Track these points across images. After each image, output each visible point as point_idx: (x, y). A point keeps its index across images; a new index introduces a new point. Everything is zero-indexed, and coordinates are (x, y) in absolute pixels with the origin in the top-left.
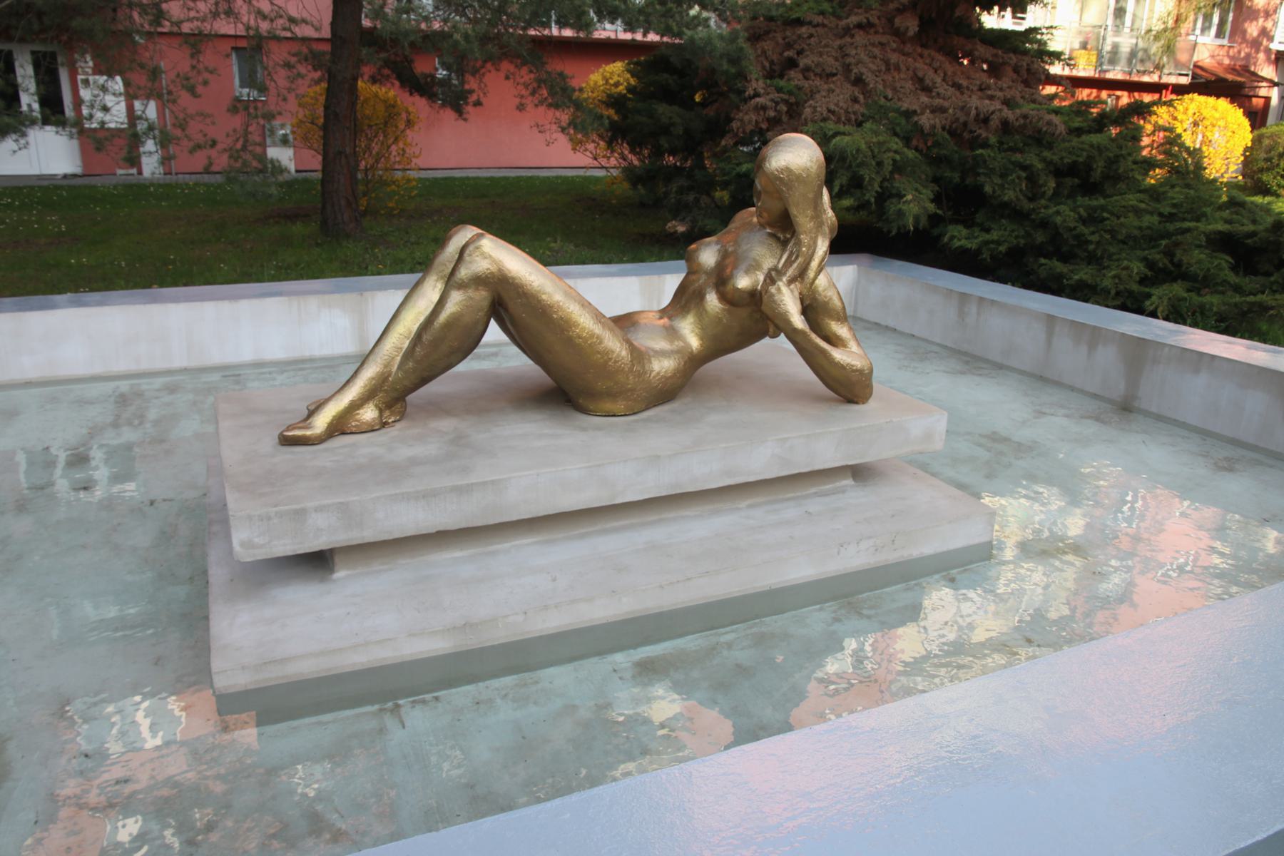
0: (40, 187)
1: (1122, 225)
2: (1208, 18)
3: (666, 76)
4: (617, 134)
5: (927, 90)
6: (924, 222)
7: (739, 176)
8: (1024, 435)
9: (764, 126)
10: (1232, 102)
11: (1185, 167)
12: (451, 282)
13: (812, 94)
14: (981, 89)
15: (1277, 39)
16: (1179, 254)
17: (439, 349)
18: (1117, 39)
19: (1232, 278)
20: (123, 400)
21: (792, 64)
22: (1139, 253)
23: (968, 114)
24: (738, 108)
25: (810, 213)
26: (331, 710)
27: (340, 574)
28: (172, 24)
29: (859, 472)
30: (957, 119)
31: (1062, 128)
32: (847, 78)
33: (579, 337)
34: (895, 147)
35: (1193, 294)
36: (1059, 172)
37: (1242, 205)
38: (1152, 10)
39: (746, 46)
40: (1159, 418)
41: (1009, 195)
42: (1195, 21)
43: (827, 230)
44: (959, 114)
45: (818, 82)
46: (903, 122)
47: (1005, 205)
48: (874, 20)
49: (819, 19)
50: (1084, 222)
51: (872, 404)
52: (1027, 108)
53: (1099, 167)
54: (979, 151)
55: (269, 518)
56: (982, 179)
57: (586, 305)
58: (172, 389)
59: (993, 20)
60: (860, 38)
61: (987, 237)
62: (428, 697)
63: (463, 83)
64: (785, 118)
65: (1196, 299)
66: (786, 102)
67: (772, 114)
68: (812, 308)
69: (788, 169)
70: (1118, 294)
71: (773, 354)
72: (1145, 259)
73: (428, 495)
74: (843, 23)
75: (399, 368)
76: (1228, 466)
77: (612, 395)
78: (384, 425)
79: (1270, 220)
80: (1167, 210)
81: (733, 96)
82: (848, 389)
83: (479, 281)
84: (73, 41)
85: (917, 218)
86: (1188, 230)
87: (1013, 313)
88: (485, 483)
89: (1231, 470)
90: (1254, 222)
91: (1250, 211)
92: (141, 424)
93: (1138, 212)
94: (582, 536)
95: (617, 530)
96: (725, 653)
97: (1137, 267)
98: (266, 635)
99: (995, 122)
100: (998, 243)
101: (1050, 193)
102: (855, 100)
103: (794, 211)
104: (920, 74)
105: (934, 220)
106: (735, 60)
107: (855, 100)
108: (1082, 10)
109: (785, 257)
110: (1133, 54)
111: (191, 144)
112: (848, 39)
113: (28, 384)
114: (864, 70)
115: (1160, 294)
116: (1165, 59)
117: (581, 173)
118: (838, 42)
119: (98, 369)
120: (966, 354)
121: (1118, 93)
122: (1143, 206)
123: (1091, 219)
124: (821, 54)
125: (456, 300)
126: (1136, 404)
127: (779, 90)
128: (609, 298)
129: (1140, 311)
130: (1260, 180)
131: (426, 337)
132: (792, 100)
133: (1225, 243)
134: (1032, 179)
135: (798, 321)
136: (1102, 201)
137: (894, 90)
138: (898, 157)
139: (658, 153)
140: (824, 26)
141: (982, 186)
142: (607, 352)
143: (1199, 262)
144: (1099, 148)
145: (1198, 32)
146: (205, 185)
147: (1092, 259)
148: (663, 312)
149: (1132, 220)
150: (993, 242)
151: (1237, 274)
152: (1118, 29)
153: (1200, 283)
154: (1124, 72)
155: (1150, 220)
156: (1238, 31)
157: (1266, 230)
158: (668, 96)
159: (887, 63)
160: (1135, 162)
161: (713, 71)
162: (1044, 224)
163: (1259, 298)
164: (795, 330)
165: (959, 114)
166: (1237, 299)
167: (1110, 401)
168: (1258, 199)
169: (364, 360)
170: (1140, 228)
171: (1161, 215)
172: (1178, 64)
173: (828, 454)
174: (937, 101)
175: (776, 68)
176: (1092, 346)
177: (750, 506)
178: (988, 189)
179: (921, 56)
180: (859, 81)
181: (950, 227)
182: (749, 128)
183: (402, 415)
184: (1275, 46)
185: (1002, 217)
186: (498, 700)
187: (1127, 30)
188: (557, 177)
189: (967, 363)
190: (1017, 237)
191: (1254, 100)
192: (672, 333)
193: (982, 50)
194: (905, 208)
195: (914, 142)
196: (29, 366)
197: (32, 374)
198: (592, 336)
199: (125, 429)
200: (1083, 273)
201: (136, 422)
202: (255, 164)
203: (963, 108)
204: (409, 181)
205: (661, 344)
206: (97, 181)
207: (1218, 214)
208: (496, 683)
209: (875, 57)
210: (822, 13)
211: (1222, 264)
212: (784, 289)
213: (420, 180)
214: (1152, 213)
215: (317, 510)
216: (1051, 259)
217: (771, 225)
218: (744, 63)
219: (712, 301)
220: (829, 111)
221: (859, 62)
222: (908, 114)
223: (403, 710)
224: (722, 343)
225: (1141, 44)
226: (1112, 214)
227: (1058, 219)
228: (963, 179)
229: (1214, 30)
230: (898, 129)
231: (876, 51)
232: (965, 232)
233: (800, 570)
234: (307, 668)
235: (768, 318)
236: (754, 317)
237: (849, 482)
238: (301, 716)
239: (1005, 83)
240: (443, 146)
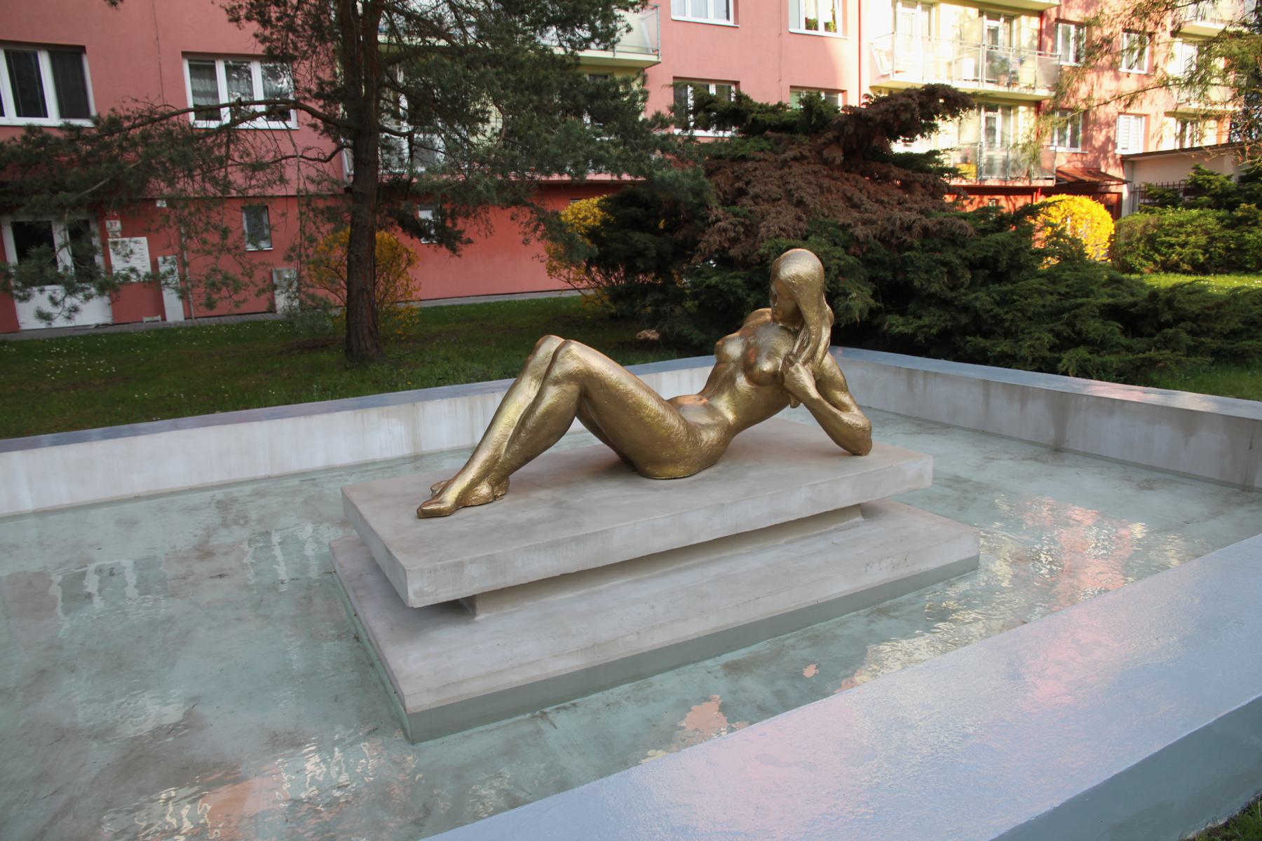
0: (82, 337)
1: (1030, 304)
2: (1062, 131)
3: (634, 209)
4: (604, 261)
5: (856, 206)
6: (865, 315)
7: (708, 287)
8: (977, 477)
9: (726, 245)
10: (1094, 199)
11: (1072, 253)
12: (545, 379)
13: (763, 217)
14: (899, 204)
15: (1119, 146)
16: (1078, 325)
17: (536, 436)
18: (991, 153)
19: (1124, 341)
20: (223, 506)
21: (742, 193)
22: (1045, 326)
23: (894, 224)
24: (703, 232)
25: (816, 308)
26: (494, 721)
27: (481, 617)
28: (238, 191)
29: (865, 510)
30: (885, 229)
31: (971, 230)
32: (790, 201)
33: (648, 416)
34: (838, 255)
35: (1095, 356)
36: (972, 266)
37: (1120, 281)
38: (1017, 126)
39: (705, 180)
40: (1086, 455)
41: (935, 287)
42: (1053, 135)
43: (828, 320)
44: (886, 224)
45: (767, 206)
46: (840, 233)
47: (931, 296)
48: (806, 153)
49: (761, 155)
50: (998, 304)
51: (872, 455)
52: (940, 216)
53: (1004, 260)
54: (907, 254)
55: (436, 571)
56: (911, 276)
57: (650, 391)
58: (261, 494)
59: (898, 147)
60: (797, 168)
61: (920, 323)
62: (567, 704)
63: (455, 225)
64: (743, 238)
65: (1097, 359)
66: (743, 224)
67: (732, 234)
68: (822, 382)
69: (798, 276)
70: (1034, 360)
71: (795, 422)
72: (1051, 331)
73: (554, 546)
74: (782, 157)
75: (507, 451)
76: (1148, 486)
77: (673, 462)
78: (495, 498)
79: (1146, 293)
80: (1063, 290)
81: (698, 222)
82: (852, 444)
83: (570, 377)
84: (99, 208)
85: (861, 311)
86: (1081, 305)
87: (955, 382)
88: (596, 533)
89: (1151, 488)
90: (1132, 294)
91: (1127, 286)
92: (246, 523)
93: (1041, 293)
94: (664, 575)
95: (688, 568)
96: (792, 652)
97: (1048, 338)
98: (430, 668)
99: (917, 229)
100: (930, 327)
101: (967, 283)
102: (799, 219)
103: (804, 308)
104: (849, 194)
105: (873, 312)
106: (697, 193)
107: (799, 219)
108: (959, 132)
109: (798, 344)
110: (1005, 164)
111: (257, 289)
112: (786, 170)
113: (137, 498)
114: (803, 194)
115: (1069, 357)
116: (1032, 168)
117: (556, 295)
118: (779, 173)
119: (195, 482)
120: (917, 418)
121: (997, 197)
122: (1044, 288)
123: (1004, 301)
124: (766, 184)
125: (552, 395)
126: (1065, 446)
127: (736, 215)
128: (671, 388)
129: (1053, 371)
130: (1125, 261)
131: (530, 424)
132: (748, 222)
133: (1112, 312)
134: (951, 273)
135: (814, 393)
136: (1010, 287)
137: (829, 208)
138: (842, 263)
139: (632, 270)
140: (765, 160)
141: (912, 282)
142: (671, 427)
143: (1096, 329)
144: (1004, 245)
145: (1056, 143)
146: (226, 326)
147: (1008, 334)
148: (702, 393)
149: (1037, 300)
150: (925, 326)
151: (1126, 336)
152: (991, 144)
153: (1098, 346)
154: (1001, 180)
155: (1050, 299)
156: (1087, 140)
157: (1145, 300)
158: (637, 225)
159: (821, 187)
160: (1032, 253)
161: (675, 203)
162: (966, 309)
163: (1148, 354)
164: (813, 400)
165: (886, 224)
166: (1130, 357)
167: (1041, 445)
168: (1126, 276)
169: (476, 450)
170: (1044, 306)
171: (1059, 294)
172: (1043, 170)
173: (846, 496)
174: (866, 216)
175: (729, 197)
176: (1023, 403)
177: (787, 543)
178: (917, 284)
179: (847, 180)
180: (800, 203)
181: (889, 317)
182: (714, 248)
183: (506, 490)
184: (1119, 152)
185: (930, 305)
186: (624, 702)
187: (998, 145)
188: (531, 300)
189: (919, 425)
190: (945, 321)
191: (1108, 196)
192: (711, 410)
193: (895, 171)
194: (851, 303)
195: (852, 250)
196: (138, 483)
197: (140, 489)
198: (658, 415)
199: (235, 528)
200: (1004, 346)
201: (242, 522)
202: (309, 302)
203: (889, 220)
204: (412, 310)
205: (705, 420)
206: (125, 328)
207: (1103, 290)
208: (618, 690)
209: (810, 183)
210: (762, 150)
211: (1114, 328)
212: (801, 369)
213: (421, 309)
214: (1052, 294)
215: (472, 562)
216: (975, 336)
217: (782, 320)
218: (706, 194)
219: (742, 382)
220: (781, 229)
221: (799, 188)
222: (844, 227)
223: (550, 716)
224: (752, 414)
225: (1011, 156)
226: (1021, 296)
227: (978, 304)
228: (894, 277)
229: (1068, 142)
230: (837, 240)
231: (811, 178)
232: (901, 320)
233: (839, 586)
234: (476, 688)
235: (789, 392)
236: (778, 392)
237: (860, 519)
238: (470, 727)
239: (918, 196)
240: (436, 280)
